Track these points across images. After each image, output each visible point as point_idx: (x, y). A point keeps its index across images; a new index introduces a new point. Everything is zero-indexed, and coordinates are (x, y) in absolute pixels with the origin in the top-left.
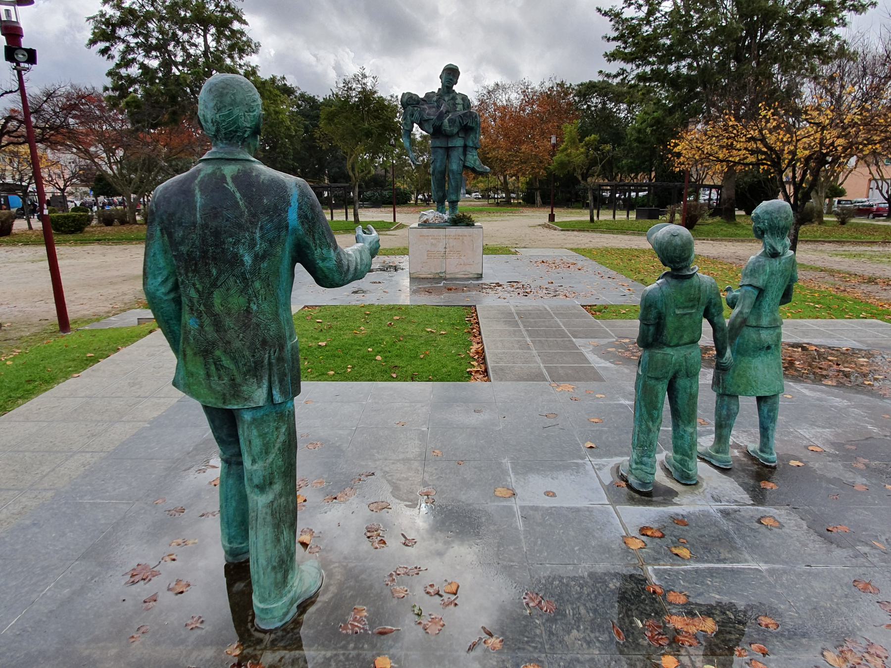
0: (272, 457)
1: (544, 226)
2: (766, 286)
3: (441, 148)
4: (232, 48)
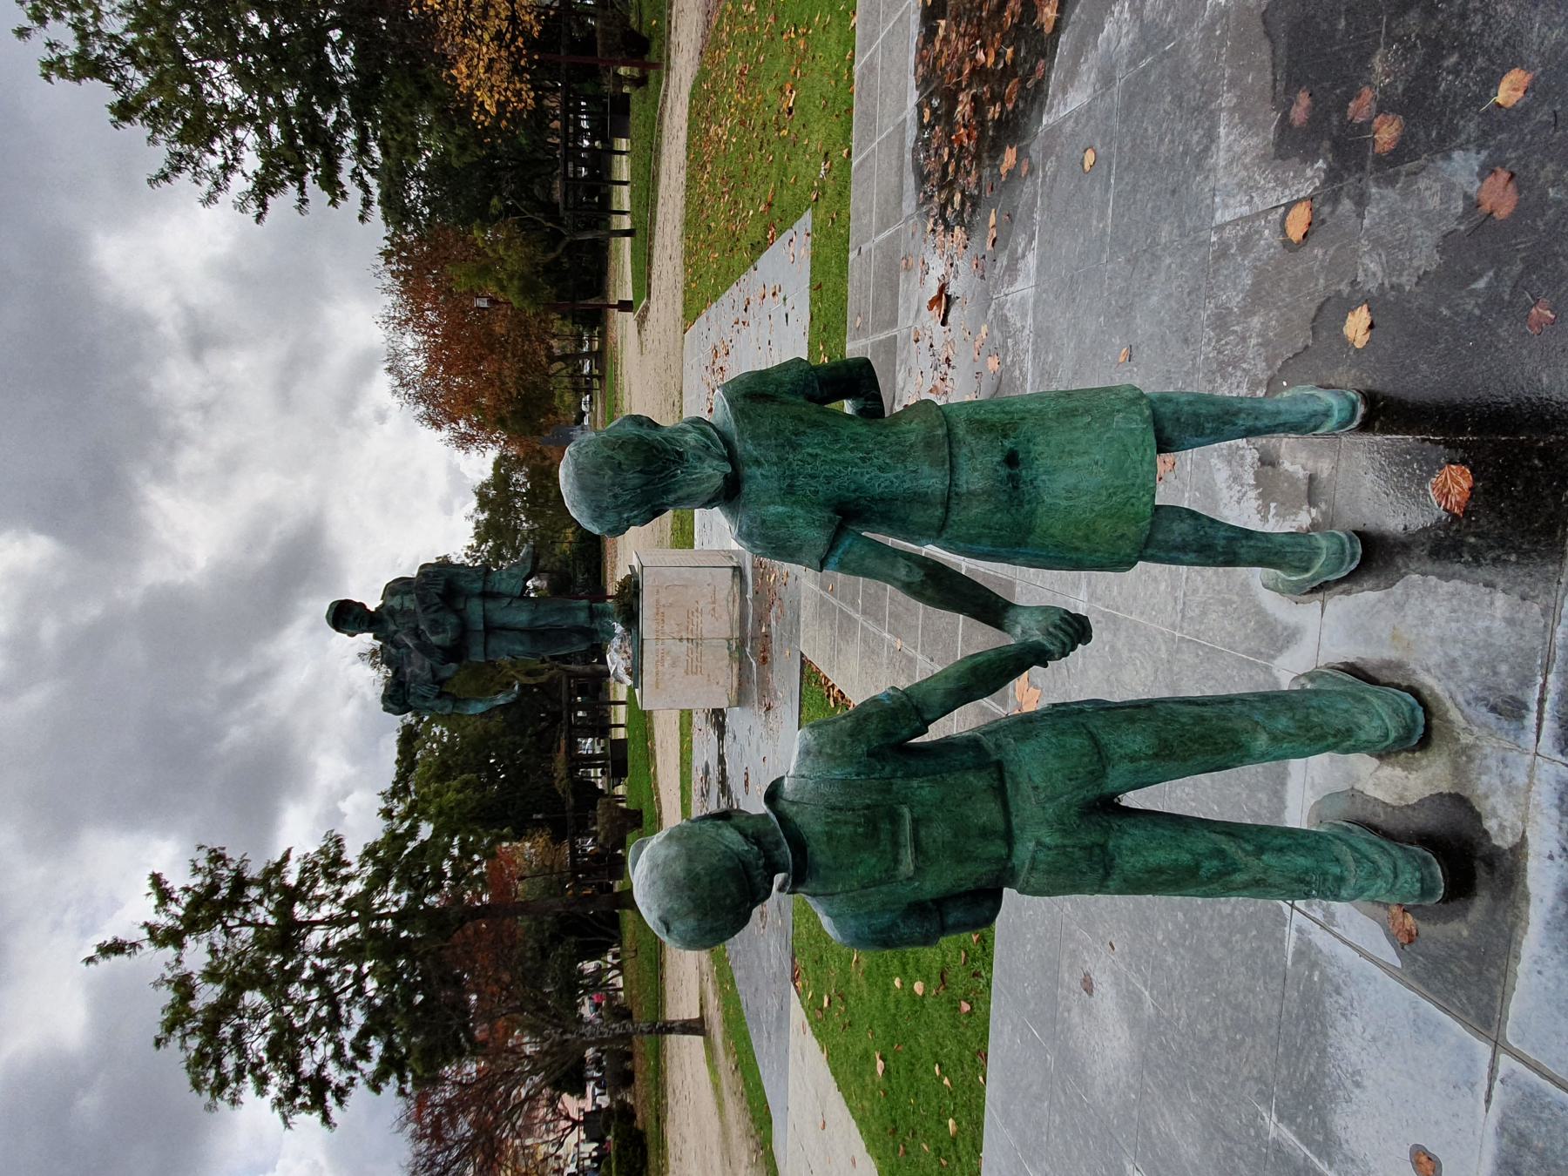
1: (642, 320)
2: (827, 503)
4: (331, 878)
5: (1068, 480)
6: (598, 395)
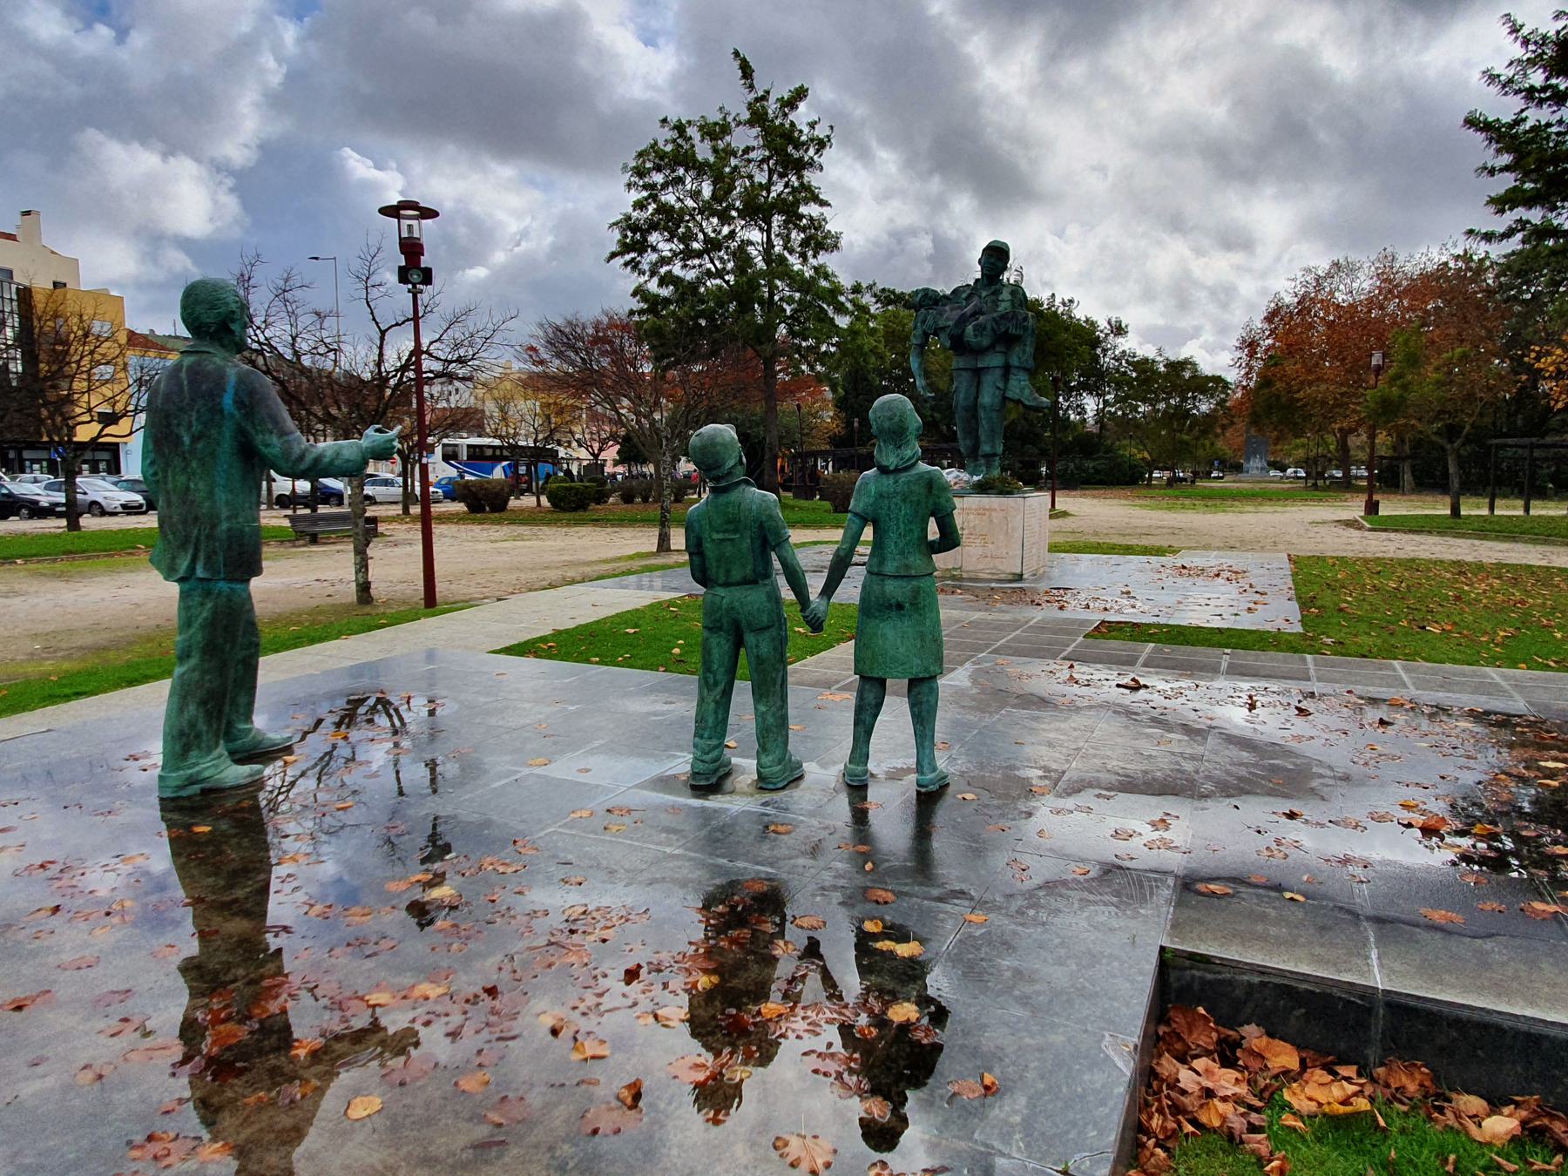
0: (192, 631)
3: (965, 369)
4: (805, 243)
5: (893, 635)
6: (1301, 484)
